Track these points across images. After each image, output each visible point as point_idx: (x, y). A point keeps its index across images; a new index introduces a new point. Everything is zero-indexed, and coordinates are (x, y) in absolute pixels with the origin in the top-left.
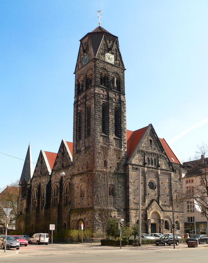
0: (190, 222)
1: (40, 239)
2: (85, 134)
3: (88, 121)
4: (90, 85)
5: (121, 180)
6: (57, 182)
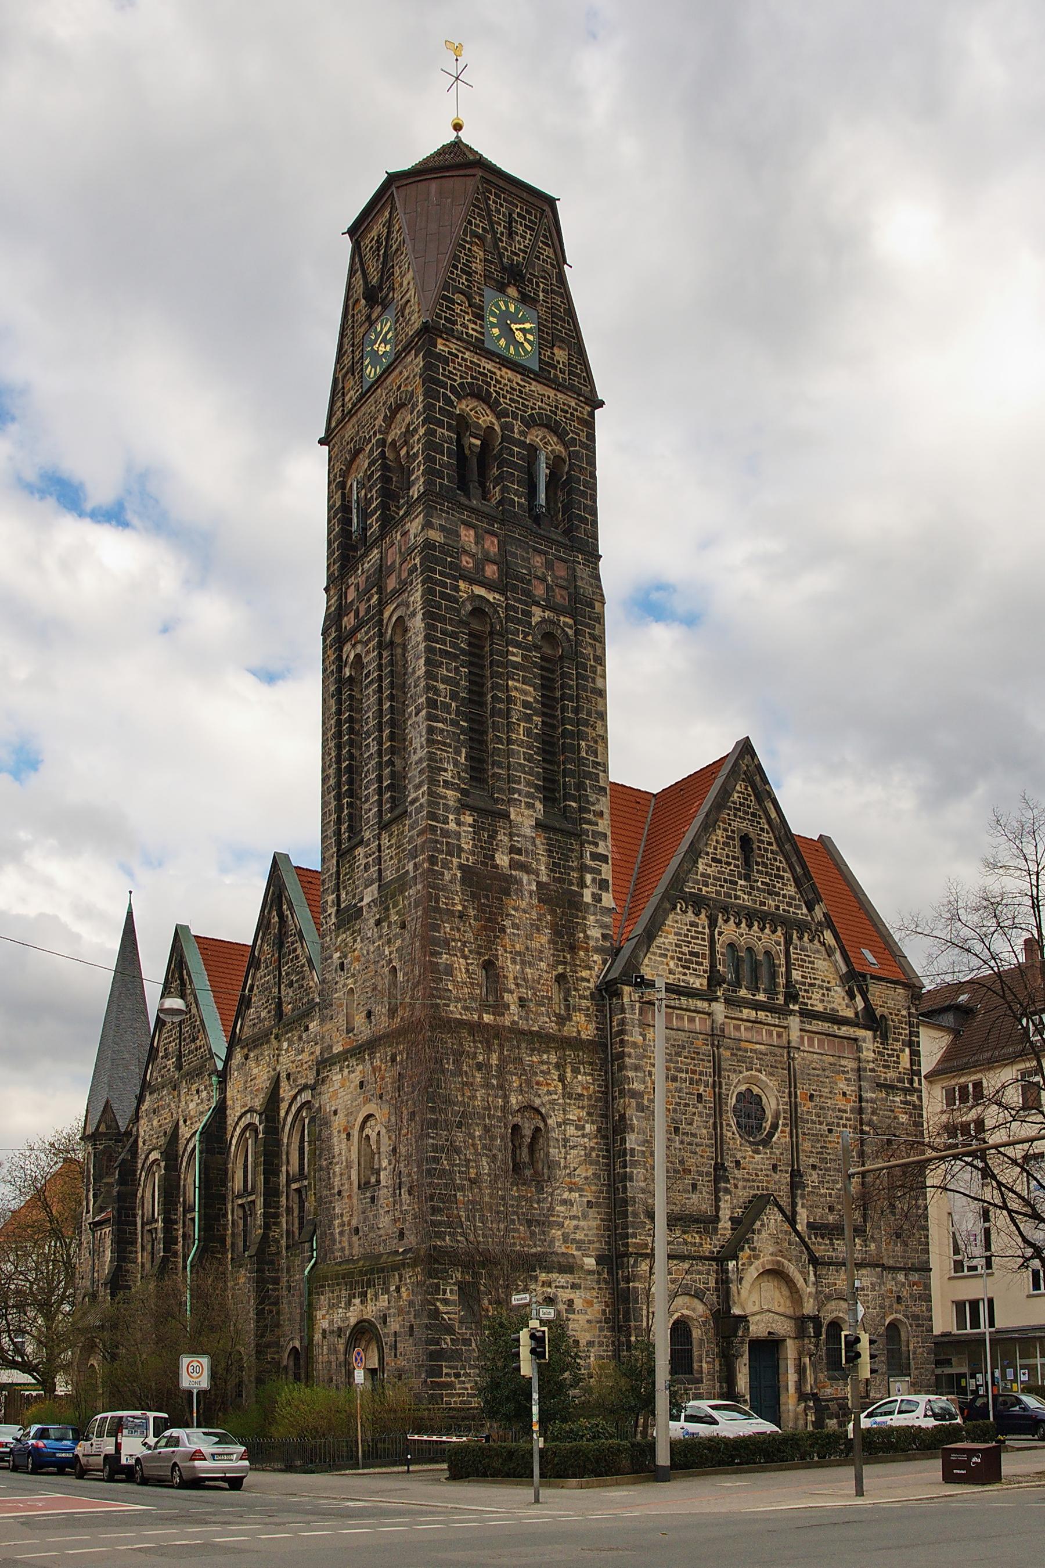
0: (969, 1331)
1: (118, 1446)
2: (380, 802)
3: (393, 723)
4: (402, 501)
5: (583, 1081)
6: (251, 1110)
